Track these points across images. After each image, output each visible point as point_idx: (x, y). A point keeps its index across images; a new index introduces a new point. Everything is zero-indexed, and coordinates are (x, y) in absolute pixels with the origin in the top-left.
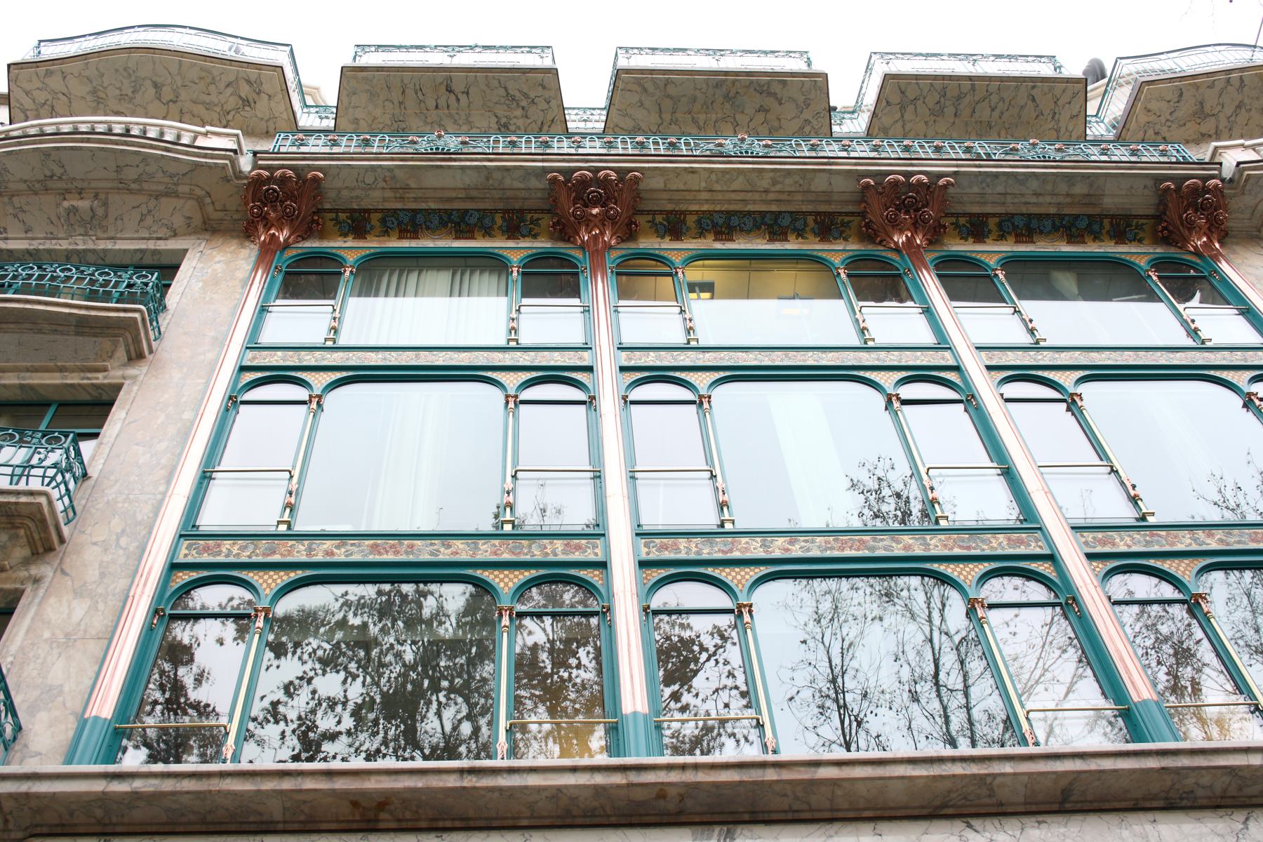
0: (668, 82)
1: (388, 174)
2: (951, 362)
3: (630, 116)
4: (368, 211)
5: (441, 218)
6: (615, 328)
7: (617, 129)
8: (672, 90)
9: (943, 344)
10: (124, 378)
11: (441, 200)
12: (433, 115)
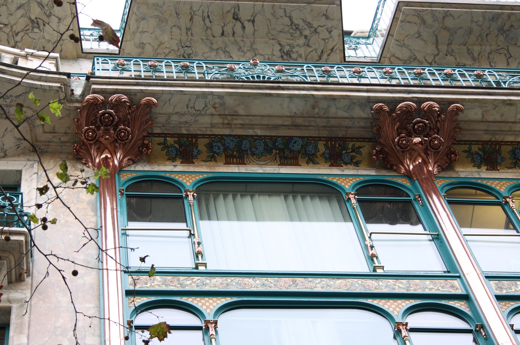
0: (446, 15)
1: (217, 101)
2: (460, 291)
3: (407, 47)
4: (196, 136)
5: (266, 144)
6: (123, 248)
7: (393, 59)
8: (449, 23)
9: (452, 271)
10: (9, 301)
11: (267, 127)
12: (219, 42)
